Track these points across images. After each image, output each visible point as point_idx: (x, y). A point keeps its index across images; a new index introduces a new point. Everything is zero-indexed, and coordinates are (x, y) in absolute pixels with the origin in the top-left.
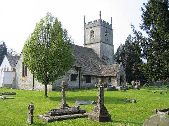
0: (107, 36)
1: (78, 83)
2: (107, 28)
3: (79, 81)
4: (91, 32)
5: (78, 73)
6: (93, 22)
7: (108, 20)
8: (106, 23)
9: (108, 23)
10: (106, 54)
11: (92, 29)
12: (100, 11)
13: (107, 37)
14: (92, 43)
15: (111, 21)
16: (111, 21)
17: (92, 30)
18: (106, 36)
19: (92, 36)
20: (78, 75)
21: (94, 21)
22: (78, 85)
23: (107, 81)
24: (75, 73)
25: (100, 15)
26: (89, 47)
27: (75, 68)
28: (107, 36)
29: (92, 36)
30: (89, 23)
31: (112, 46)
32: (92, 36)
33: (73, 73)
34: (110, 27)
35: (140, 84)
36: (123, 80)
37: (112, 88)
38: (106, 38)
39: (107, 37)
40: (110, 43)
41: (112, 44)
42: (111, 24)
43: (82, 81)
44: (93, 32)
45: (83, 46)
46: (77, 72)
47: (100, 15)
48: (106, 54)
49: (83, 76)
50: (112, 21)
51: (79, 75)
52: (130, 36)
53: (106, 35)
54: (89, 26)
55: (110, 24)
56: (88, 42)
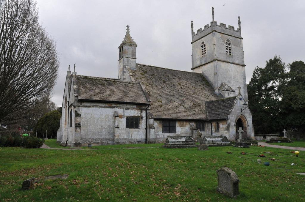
0: (230, 50)
1: (145, 134)
2: (231, 36)
3: (146, 129)
4: (202, 47)
5: (144, 114)
6: (203, 29)
7: (231, 22)
8: (227, 27)
9: (231, 28)
10: (229, 81)
11: (203, 40)
12: (213, 8)
13: (230, 52)
14: (203, 63)
15: (239, 22)
16: (239, 22)
17: (203, 43)
18: (228, 50)
19: (204, 53)
20: (142, 118)
21: (205, 27)
22: (144, 137)
23: (214, 129)
24: (136, 115)
25: (213, 14)
26: (199, 71)
27: (135, 107)
28: (230, 50)
29: (203, 51)
30: (198, 31)
31: (241, 67)
32: (203, 51)
33: (132, 115)
34: (238, 33)
35: (287, 133)
36: (246, 127)
37: (183, 142)
38: (229, 53)
39: (230, 52)
40: (237, 62)
41: (241, 64)
42: (239, 29)
43: (150, 130)
44: (205, 46)
45: (191, 71)
46: (140, 112)
47: (213, 14)
48: (229, 81)
49: (153, 119)
50: (241, 24)
51: (144, 118)
52: (208, 24)
53: (228, 48)
54: (198, 37)
55: (236, 29)
56: (198, 63)
